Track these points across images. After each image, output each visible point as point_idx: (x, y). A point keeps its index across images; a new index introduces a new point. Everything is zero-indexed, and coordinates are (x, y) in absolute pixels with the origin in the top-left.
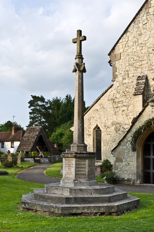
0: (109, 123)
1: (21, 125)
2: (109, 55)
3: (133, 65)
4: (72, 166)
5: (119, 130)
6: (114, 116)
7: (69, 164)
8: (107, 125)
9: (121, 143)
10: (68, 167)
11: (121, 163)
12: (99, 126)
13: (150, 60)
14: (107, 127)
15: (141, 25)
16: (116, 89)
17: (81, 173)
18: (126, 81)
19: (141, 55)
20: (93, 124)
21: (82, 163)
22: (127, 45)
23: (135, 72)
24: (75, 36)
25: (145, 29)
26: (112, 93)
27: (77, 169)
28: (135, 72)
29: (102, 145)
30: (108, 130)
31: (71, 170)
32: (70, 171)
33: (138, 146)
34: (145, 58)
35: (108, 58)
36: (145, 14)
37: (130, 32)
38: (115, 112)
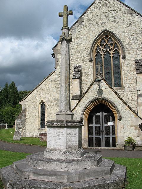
0: (52, 99)
2: (53, 50)
4: (61, 135)
7: (58, 133)
8: (51, 100)
13: (83, 55)
14: (50, 102)
15: (77, 32)
16: (58, 74)
20: (39, 99)
21: (73, 132)
23: (73, 63)
24: (62, 10)
26: (55, 77)
27: (68, 139)
28: (73, 63)
29: (46, 116)
33: (85, 117)
34: (80, 53)
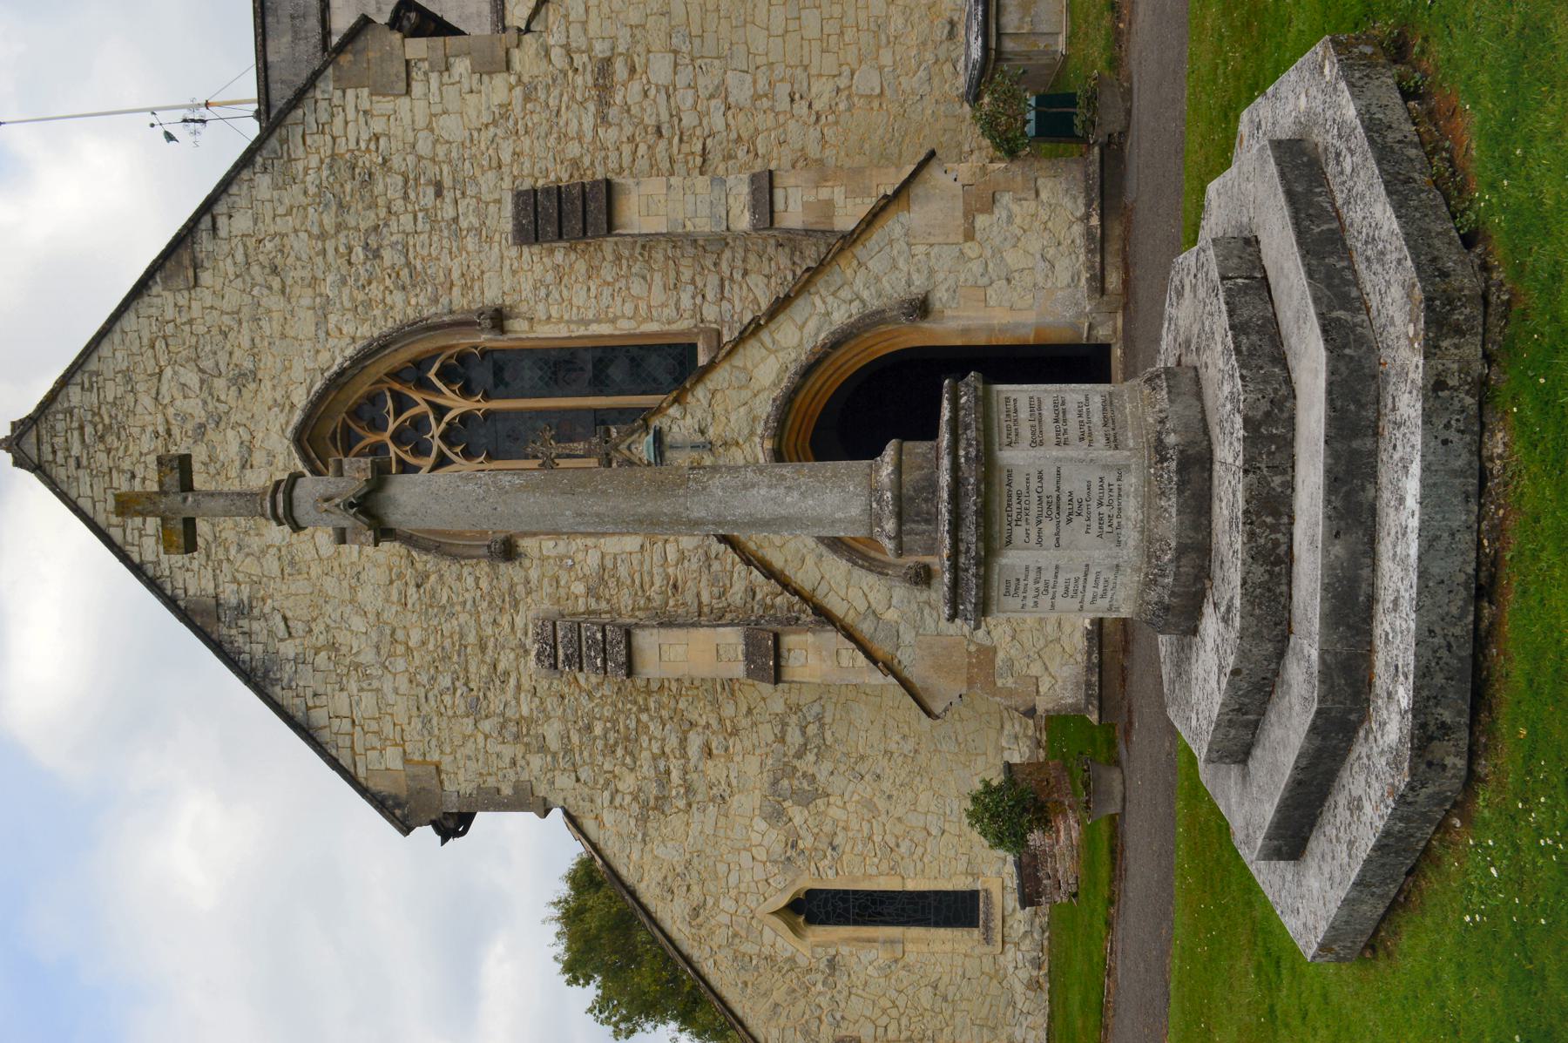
1: (554, 939)
3: (475, 693)
5: (813, 779)
6: (735, 805)
8: (778, 848)
9: (879, 655)
10: (1063, 517)
11: (1001, 655)
12: (784, 900)
15: (288, 649)
17: (1097, 419)
18: (552, 732)
19: (431, 647)
22: (374, 726)
25: (313, 625)
30: (806, 842)
31: (1080, 493)
32: (1094, 504)
35: (425, 834)
36: (240, 623)
37: (308, 708)
38: (713, 800)
